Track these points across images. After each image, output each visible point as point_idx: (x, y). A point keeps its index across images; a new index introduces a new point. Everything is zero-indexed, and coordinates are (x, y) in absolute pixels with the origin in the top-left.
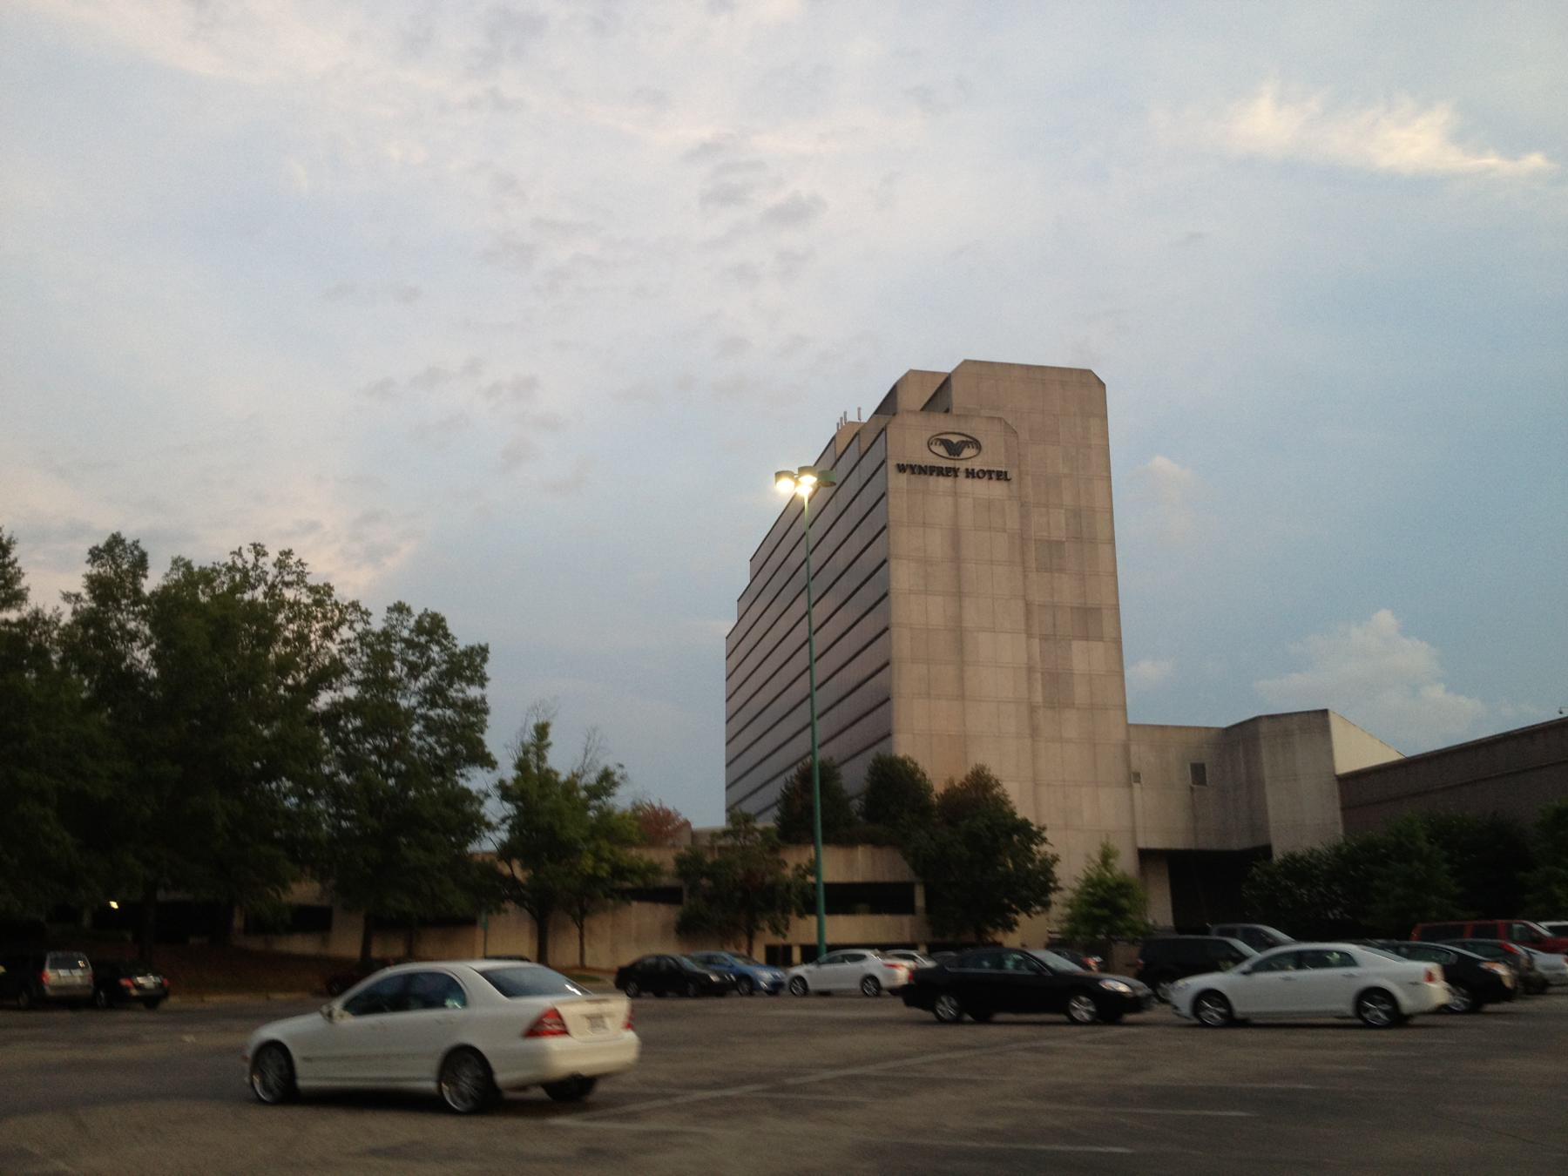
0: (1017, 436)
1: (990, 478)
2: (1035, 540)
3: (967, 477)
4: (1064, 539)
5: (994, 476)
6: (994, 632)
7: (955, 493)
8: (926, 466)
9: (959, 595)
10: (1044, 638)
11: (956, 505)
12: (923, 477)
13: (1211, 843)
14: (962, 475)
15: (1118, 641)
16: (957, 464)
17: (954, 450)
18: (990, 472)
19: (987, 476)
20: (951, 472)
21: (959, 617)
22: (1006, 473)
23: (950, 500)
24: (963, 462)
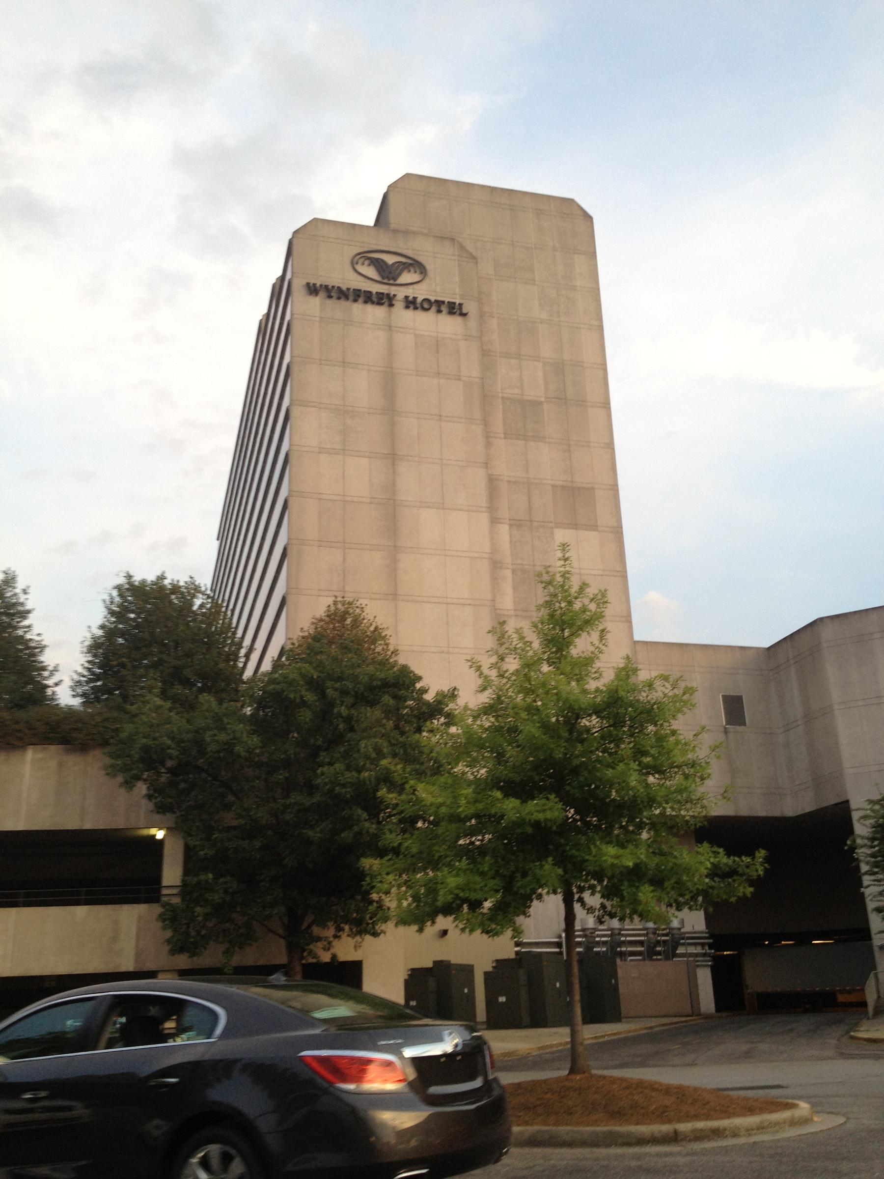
0: (477, 263)
1: (439, 311)
2: (503, 398)
3: (407, 307)
4: (543, 399)
5: (444, 308)
6: (443, 509)
7: (390, 327)
8: (348, 289)
9: (392, 458)
10: (515, 524)
11: (390, 342)
12: (343, 303)
13: (138, 970)
14: (399, 305)
15: (617, 532)
16: (393, 290)
17: (388, 273)
18: (439, 303)
19: (434, 309)
20: (384, 300)
21: (391, 487)
22: (460, 305)
23: (382, 335)
24: (402, 289)
